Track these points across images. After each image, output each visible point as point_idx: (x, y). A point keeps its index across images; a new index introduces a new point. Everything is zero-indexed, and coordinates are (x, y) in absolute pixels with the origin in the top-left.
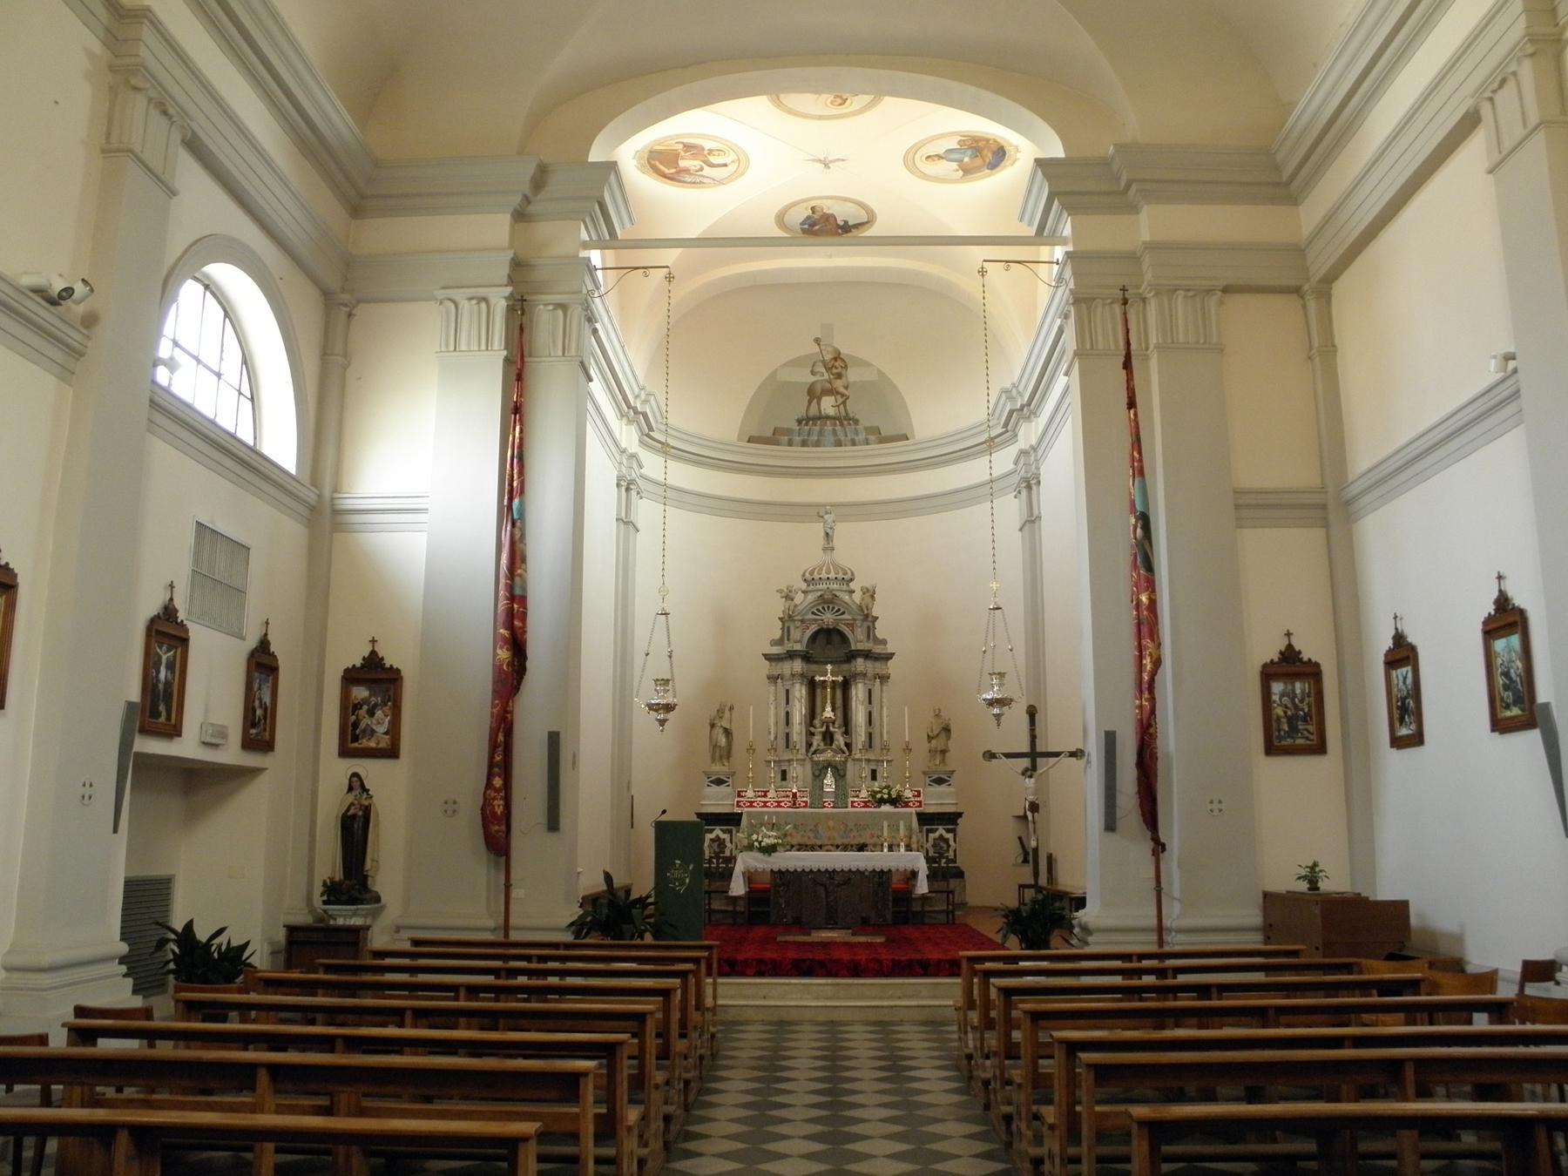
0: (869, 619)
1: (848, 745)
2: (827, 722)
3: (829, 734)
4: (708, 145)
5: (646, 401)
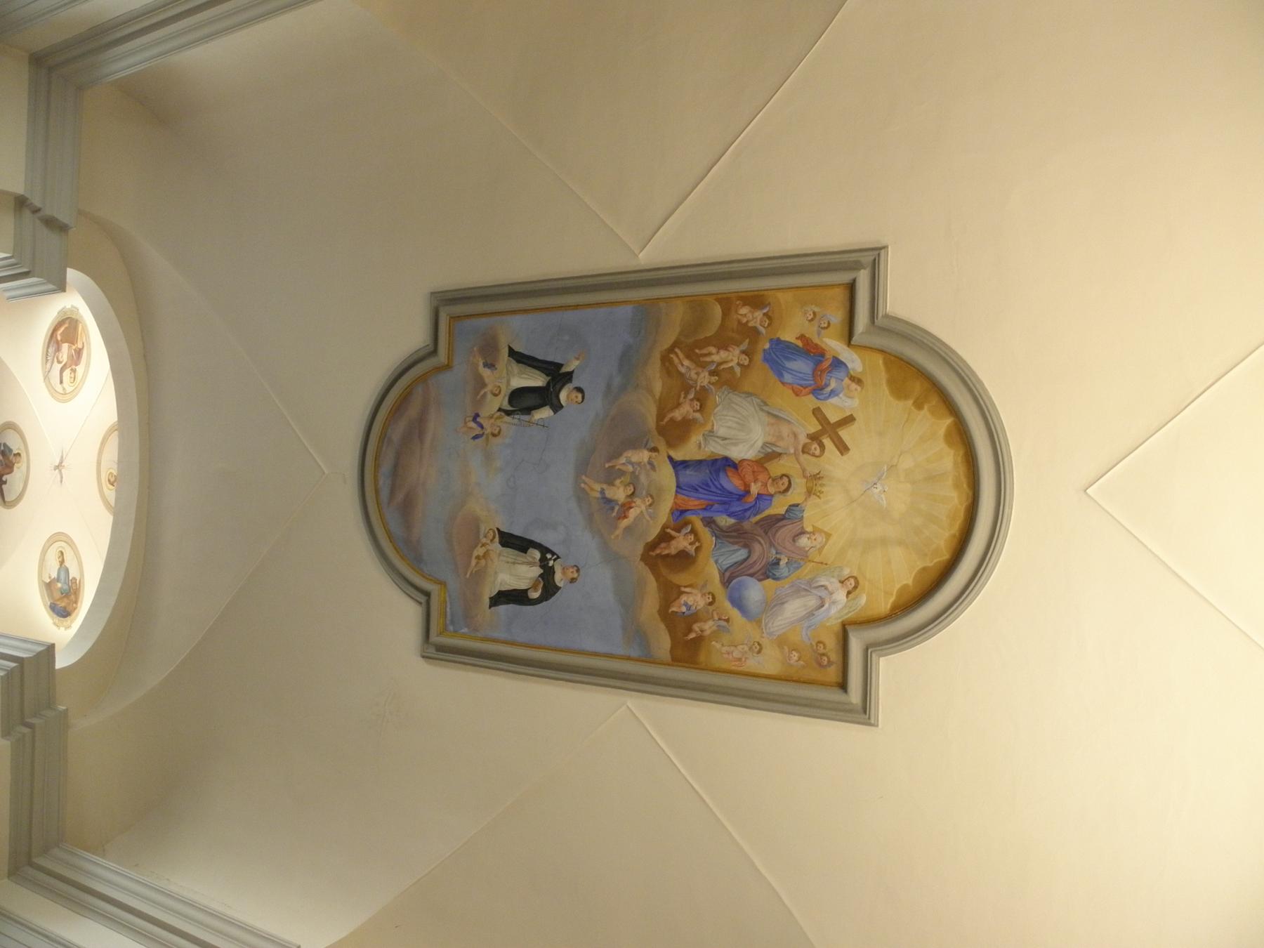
4: (80, 369)
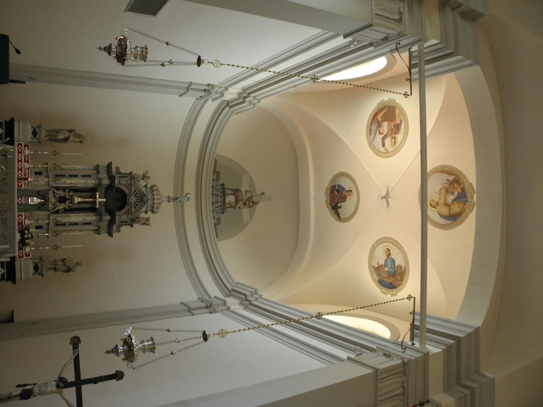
0: (131, 222)
1: (58, 212)
2: (71, 199)
3: (64, 200)
4: (399, 137)
5: (250, 103)
